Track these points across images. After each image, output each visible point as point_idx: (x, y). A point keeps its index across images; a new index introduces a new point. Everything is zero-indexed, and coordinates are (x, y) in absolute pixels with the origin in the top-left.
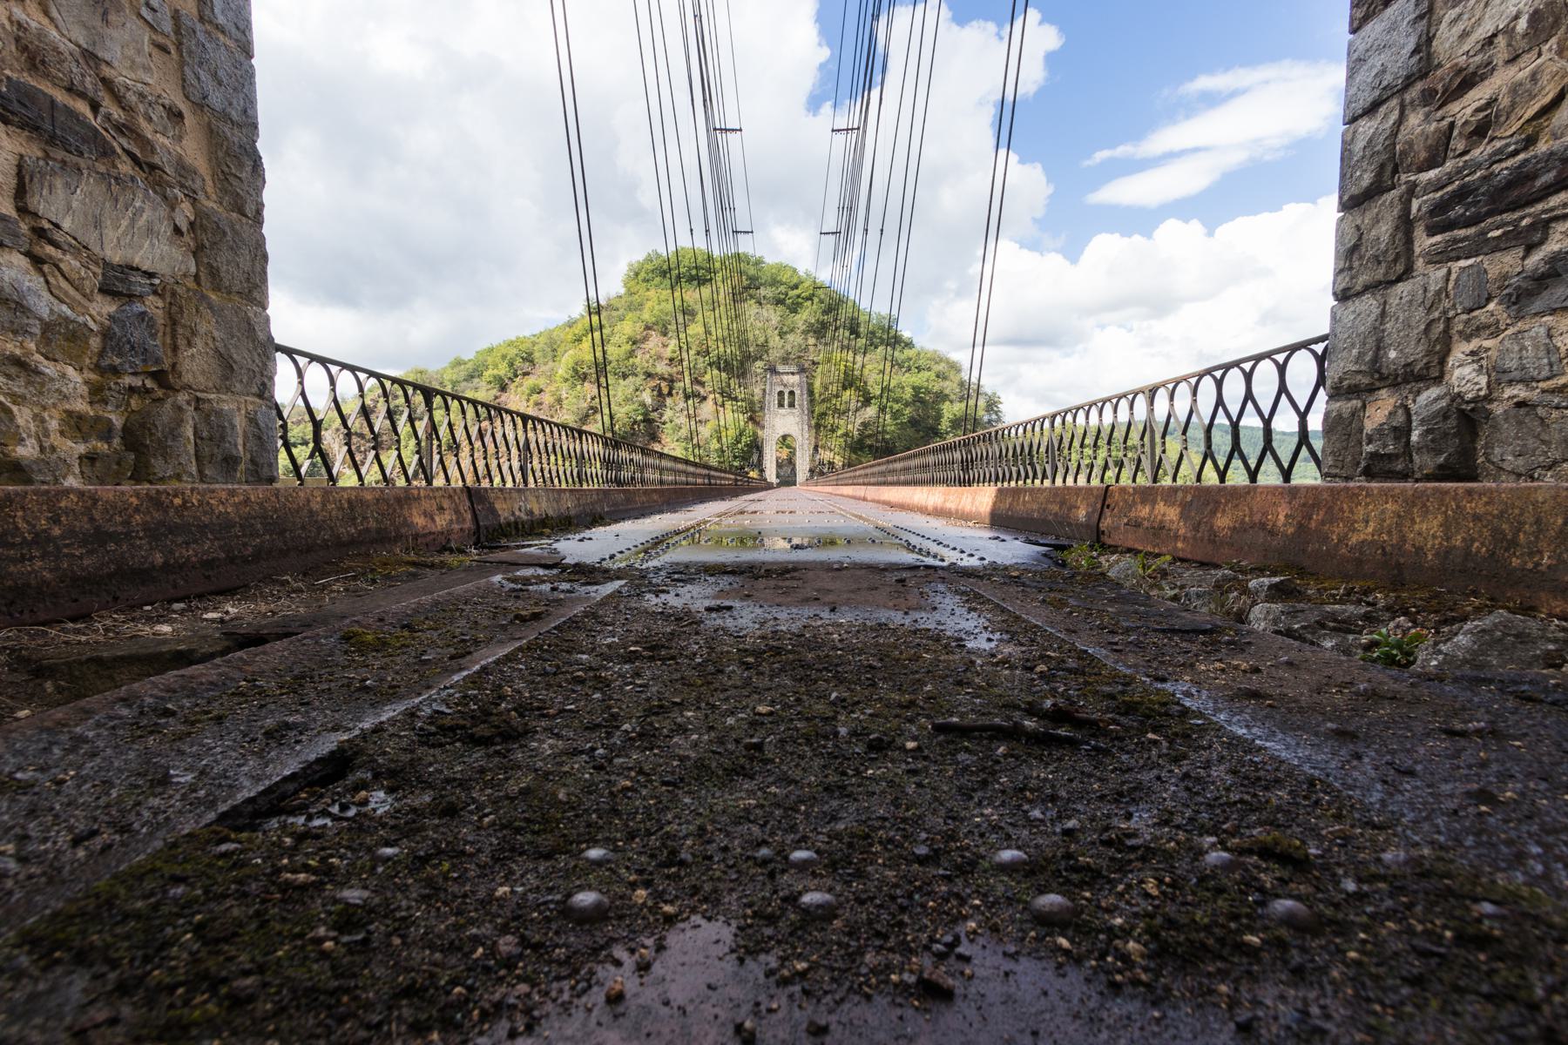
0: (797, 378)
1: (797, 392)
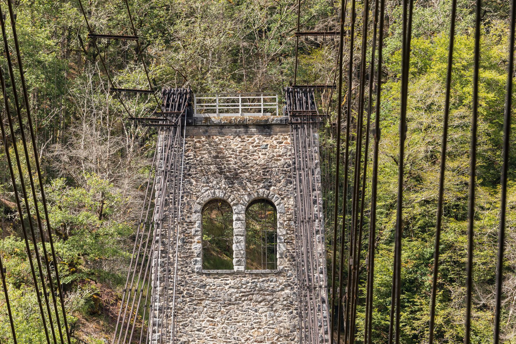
0: (279, 147)
1: (285, 206)
